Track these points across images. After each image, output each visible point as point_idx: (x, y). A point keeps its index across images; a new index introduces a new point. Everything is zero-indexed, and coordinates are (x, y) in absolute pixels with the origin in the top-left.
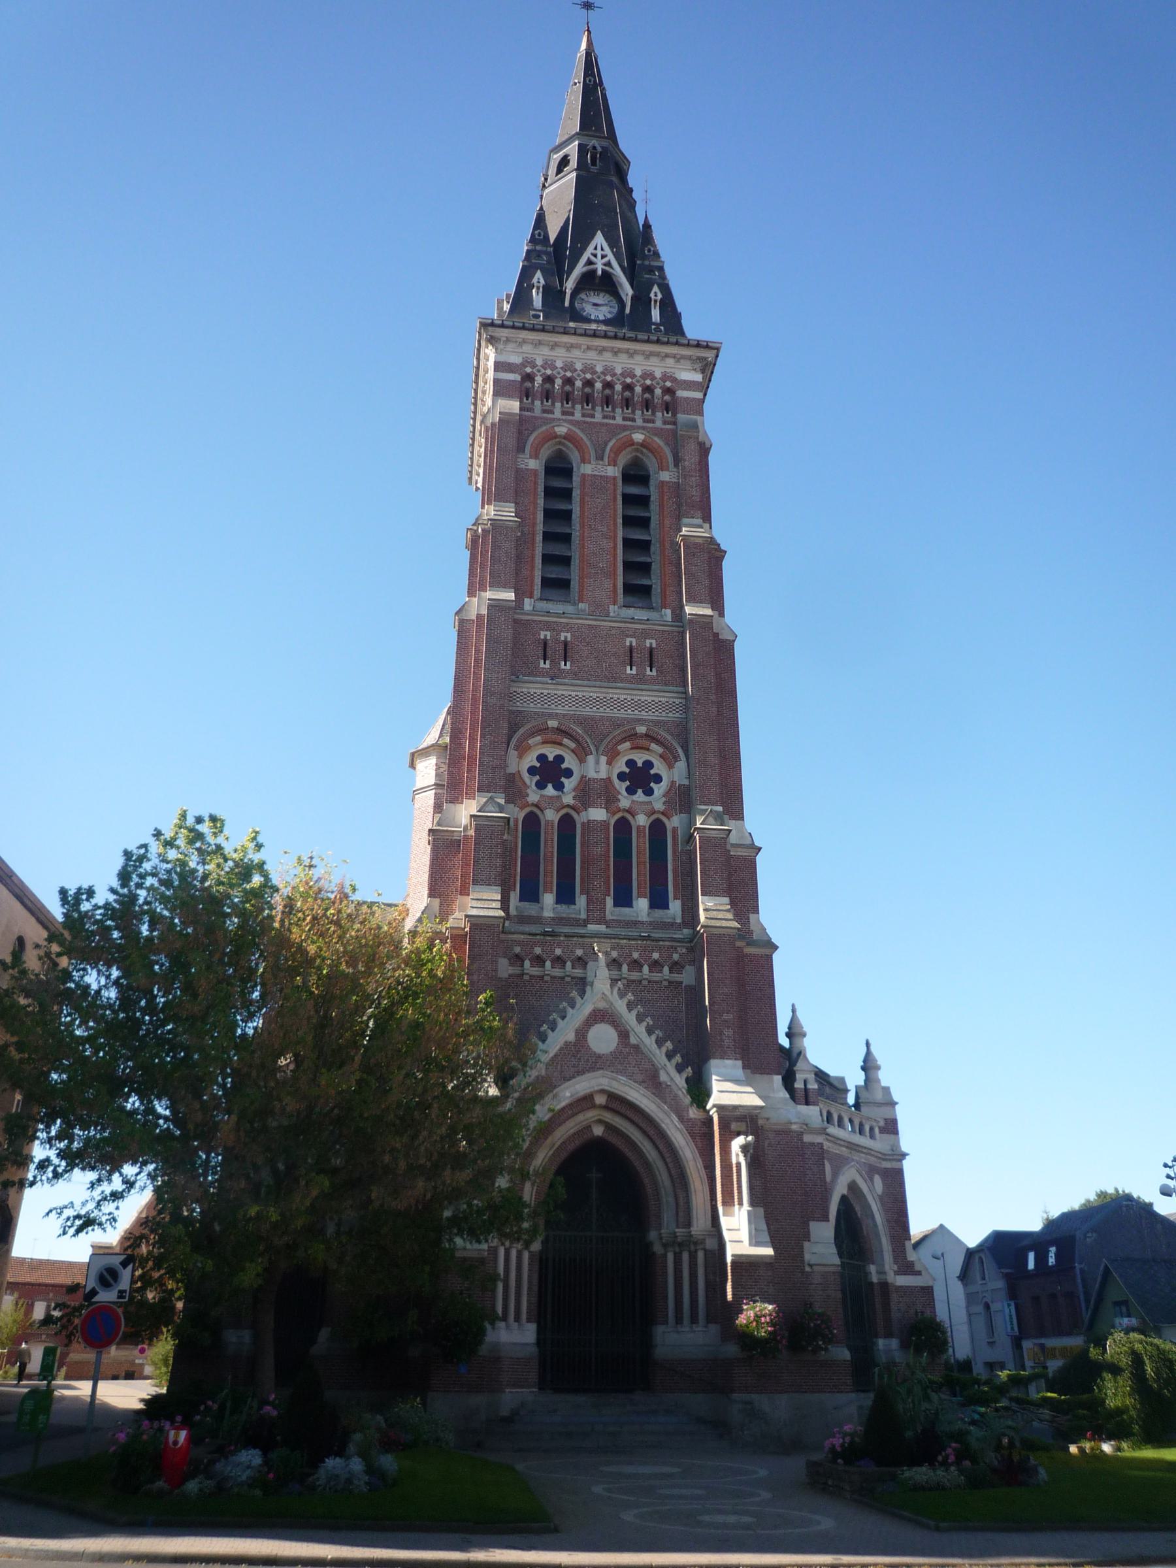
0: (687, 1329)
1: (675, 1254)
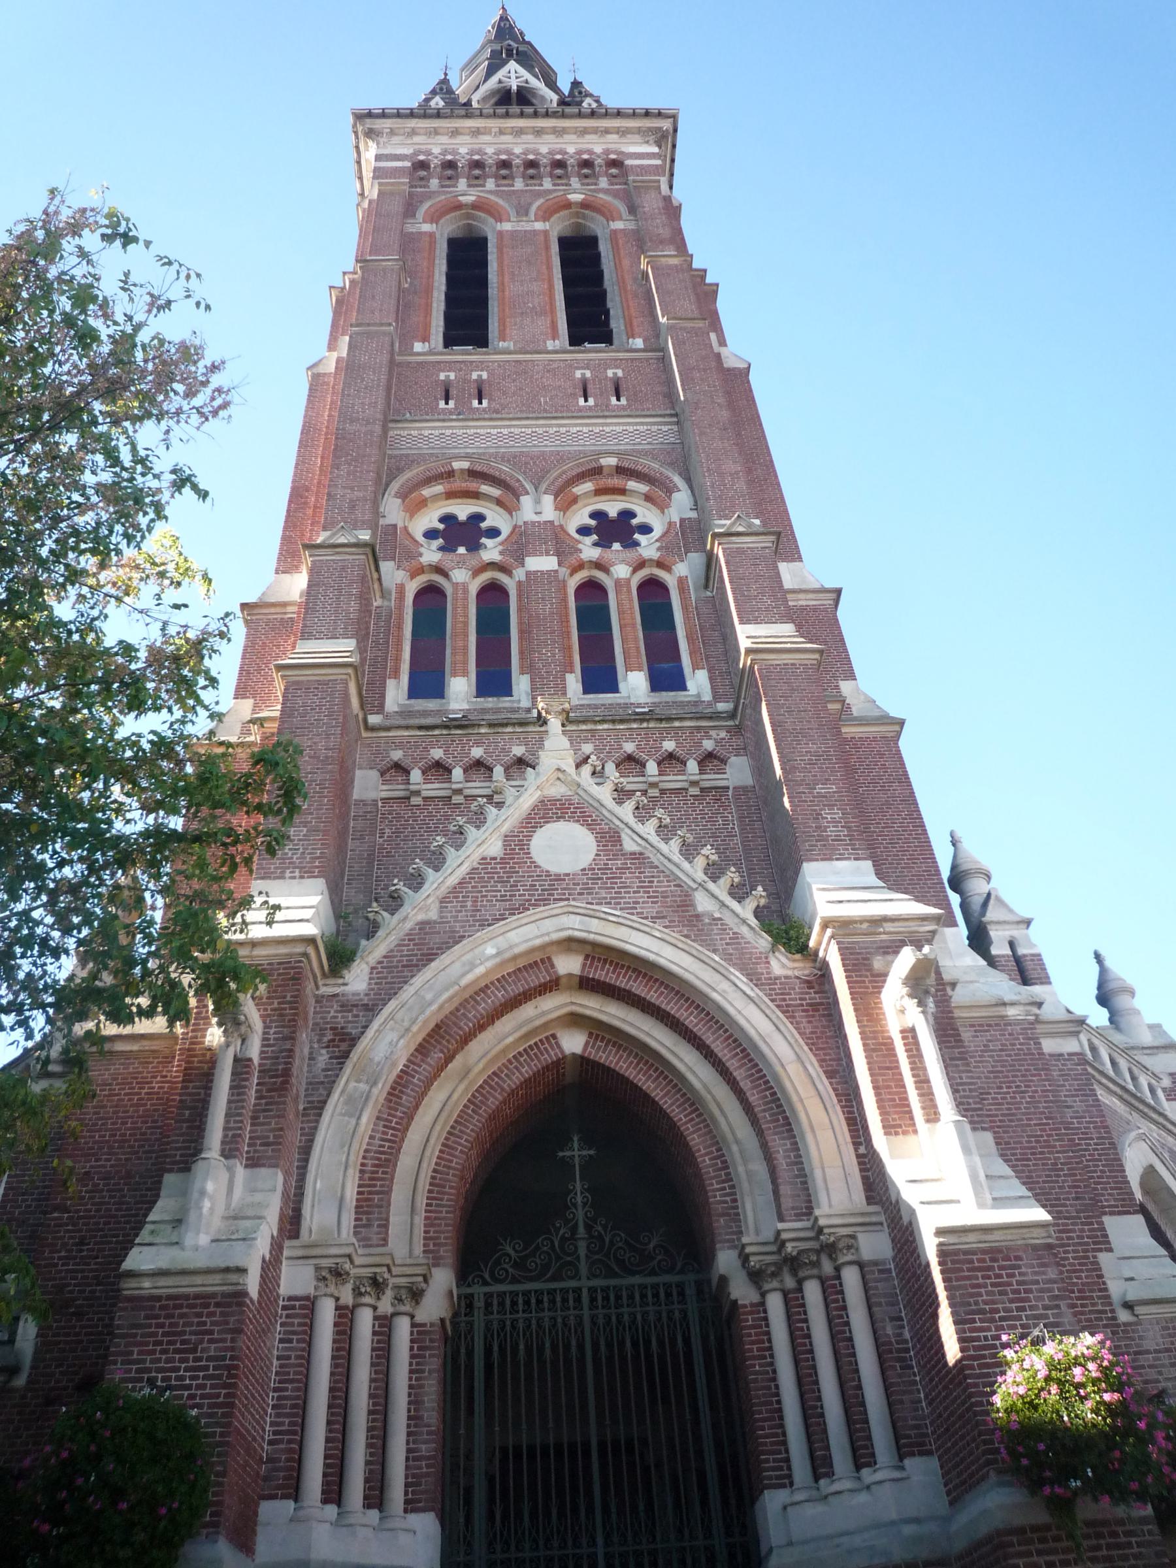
0: (847, 1485)
1: (785, 1294)
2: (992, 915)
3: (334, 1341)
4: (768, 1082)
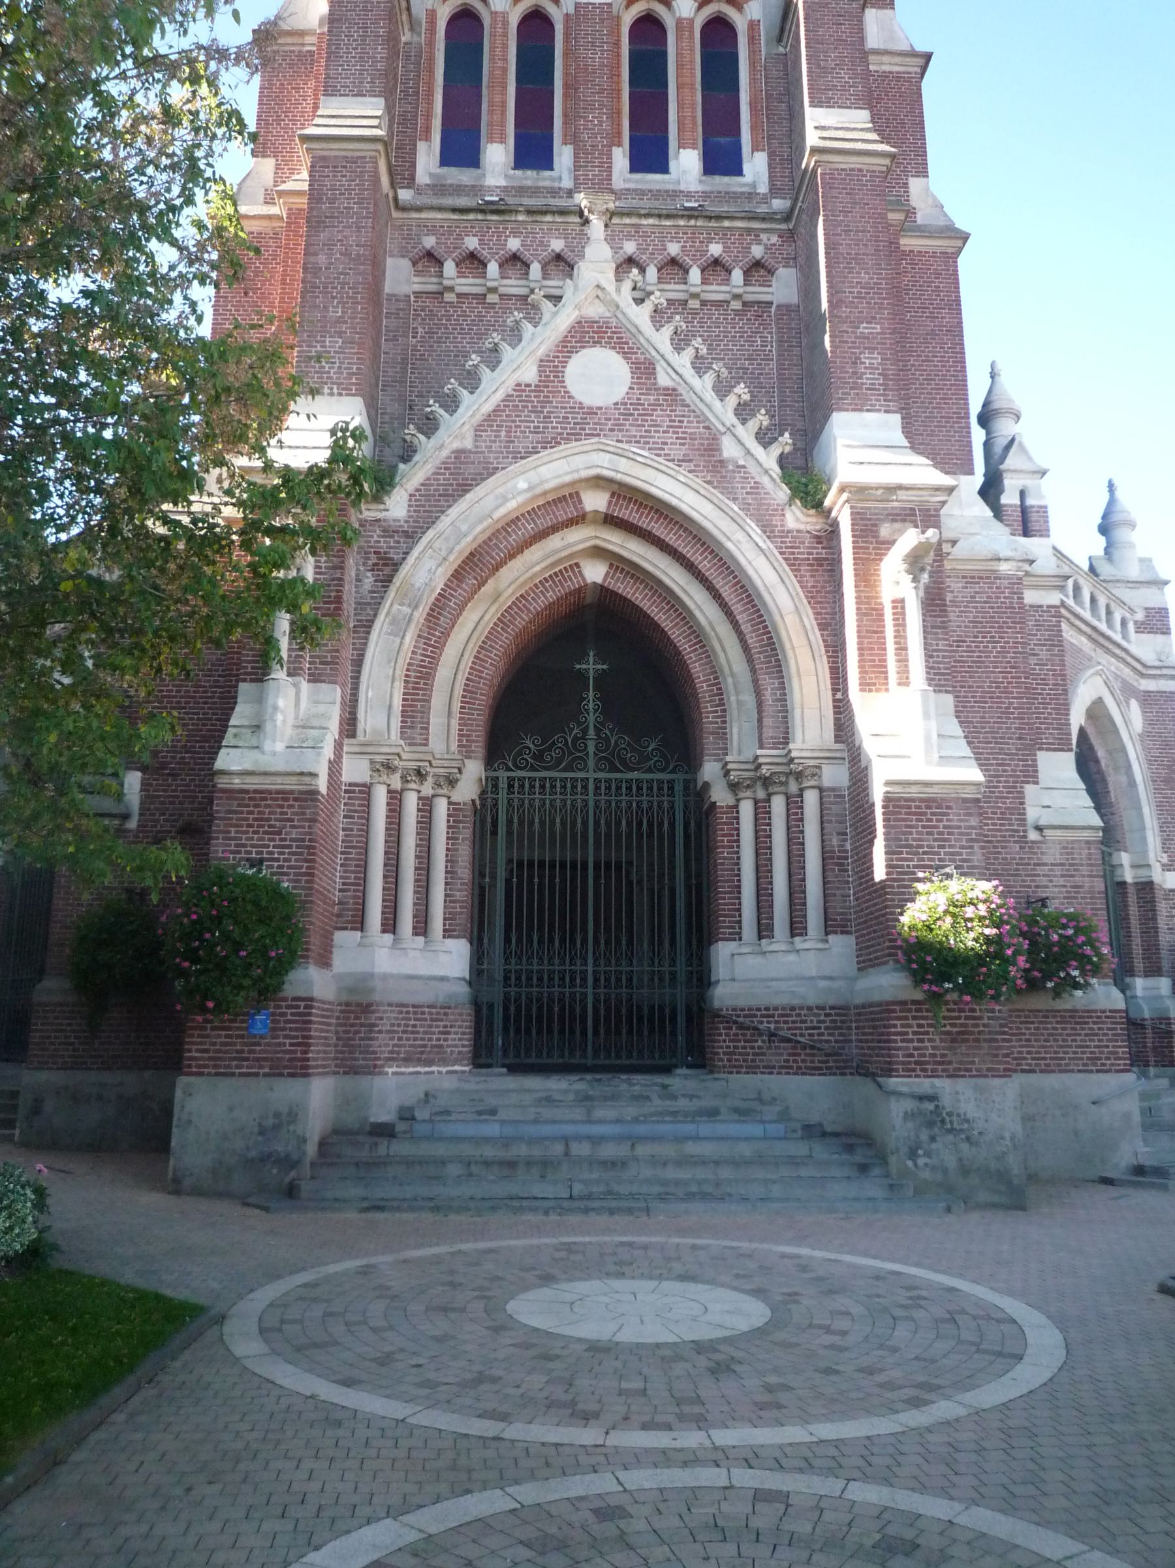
0: (783, 947)
2: (1011, 462)
3: (387, 817)
4: (766, 627)
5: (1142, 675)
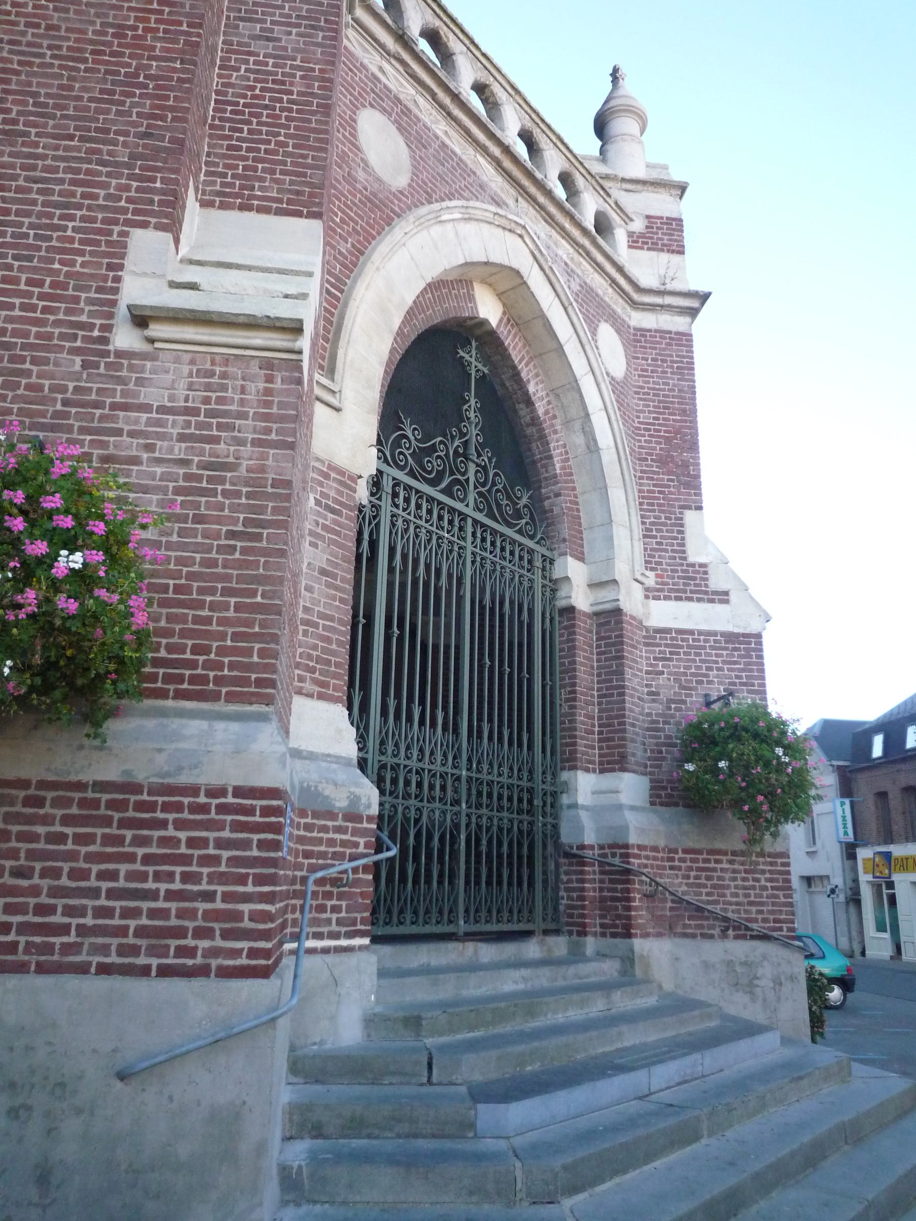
5: (635, 305)
